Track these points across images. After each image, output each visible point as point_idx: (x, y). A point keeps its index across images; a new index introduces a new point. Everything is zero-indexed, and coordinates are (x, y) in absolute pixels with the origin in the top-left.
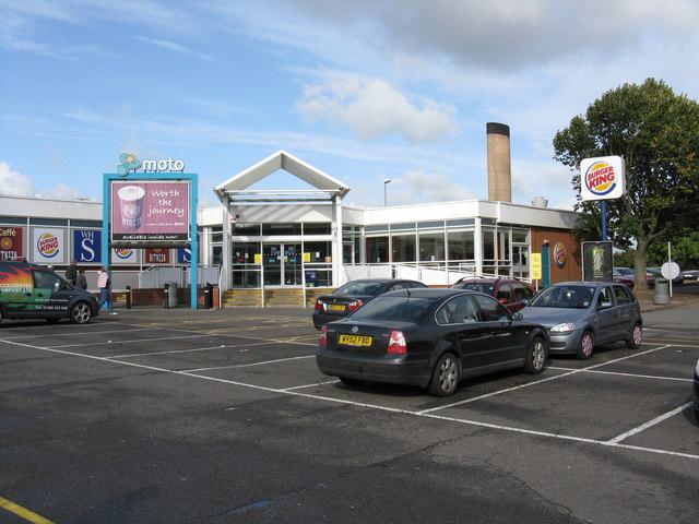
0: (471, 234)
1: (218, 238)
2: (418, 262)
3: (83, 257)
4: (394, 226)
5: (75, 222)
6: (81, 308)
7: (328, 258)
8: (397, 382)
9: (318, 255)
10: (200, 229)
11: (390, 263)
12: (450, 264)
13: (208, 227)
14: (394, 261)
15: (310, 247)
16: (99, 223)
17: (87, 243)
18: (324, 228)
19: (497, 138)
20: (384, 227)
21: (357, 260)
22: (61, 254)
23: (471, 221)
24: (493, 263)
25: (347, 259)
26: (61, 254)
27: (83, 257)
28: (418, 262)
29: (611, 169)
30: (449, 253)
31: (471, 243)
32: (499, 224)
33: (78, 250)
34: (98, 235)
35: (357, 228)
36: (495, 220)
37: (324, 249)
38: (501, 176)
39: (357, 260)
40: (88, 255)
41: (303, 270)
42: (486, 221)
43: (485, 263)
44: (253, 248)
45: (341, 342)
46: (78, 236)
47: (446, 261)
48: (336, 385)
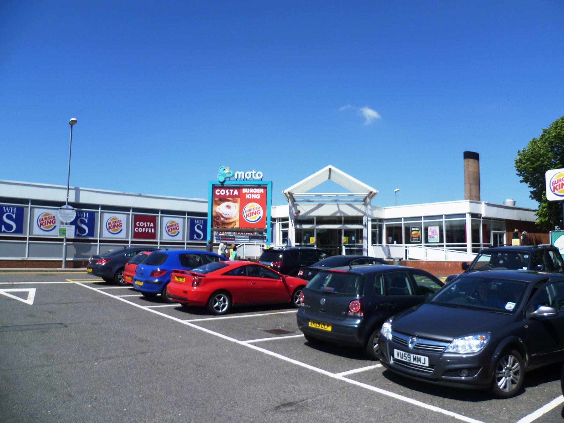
0: (465, 225)
1: (286, 226)
2: (423, 244)
3: (195, 237)
4: (406, 219)
5: (190, 214)
6: (220, 298)
7: (360, 241)
8: (450, 365)
9: (353, 238)
10: (274, 220)
11: (404, 244)
12: (447, 246)
13: (468, 213)
14: (406, 243)
15: (349, 233)
16: (205, 215)
17: (199, 228)
18: (358, 220)
19: (471, 161)
20: (400, 219)
21: (465, 246)
22: (180, 235)
23: (464, 215)
24: (479, 246)
25: (374, 242)
26: (180, 235)
27: (195, 237)
28: (423, 244)
29: (54, 217)
30: (447, 237)
31: (464, 232)
32: (483, 218)
33: (192, 233)
34: (205, 222)
35: (381, 220)
36: (481, 215)
37: (359, 234)
38: (474, 188)
39: (465, 246)
40: (199, 235)
41: (344, 248)
42: (474, 215)
43: (473, 246)
44: (310, 233)
45: (344, 312)
46: (192, 223)
47: (445, 244)
48: (141, 298)
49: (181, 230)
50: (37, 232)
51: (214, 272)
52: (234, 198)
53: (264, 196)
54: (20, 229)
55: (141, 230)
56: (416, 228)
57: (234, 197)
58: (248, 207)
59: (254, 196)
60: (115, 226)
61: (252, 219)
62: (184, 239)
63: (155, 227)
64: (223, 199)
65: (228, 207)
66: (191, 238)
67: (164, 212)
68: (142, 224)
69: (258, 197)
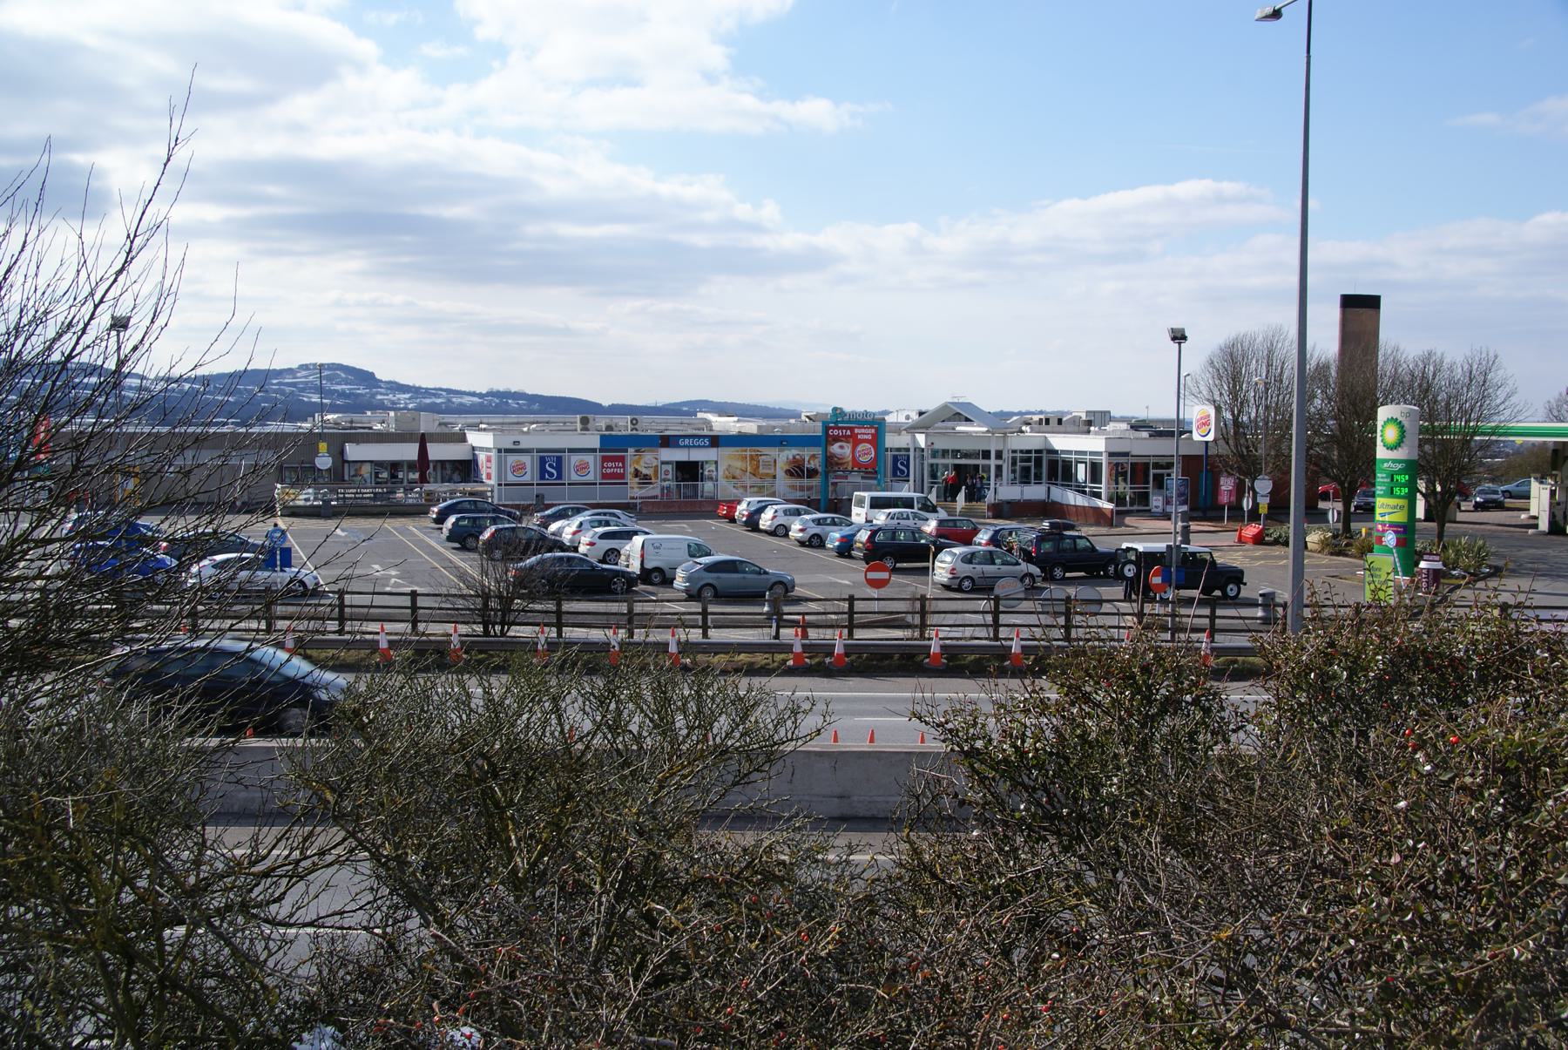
23: (1100, 454)
26: (592, 473)
40: (551, 475)
43: (436, 482)
49: (528, 469)
50: (575, 478)
51: (306, 521)
52: (846, 438)
53: (875, 436)
54: (560, 477)
55: (609, 471)
56: (692, 451)
57: (846, 437)
58: (860, 448)
59: (866, 437)
60: (583, 467)
61: (864, 459)
62: (533, 479)
63: (623, 467)
64: (836, 439)
65: (841, 447)
66: (542, 478)
67: (572, 451)
68: (610, 464)
69: (870, 437)
